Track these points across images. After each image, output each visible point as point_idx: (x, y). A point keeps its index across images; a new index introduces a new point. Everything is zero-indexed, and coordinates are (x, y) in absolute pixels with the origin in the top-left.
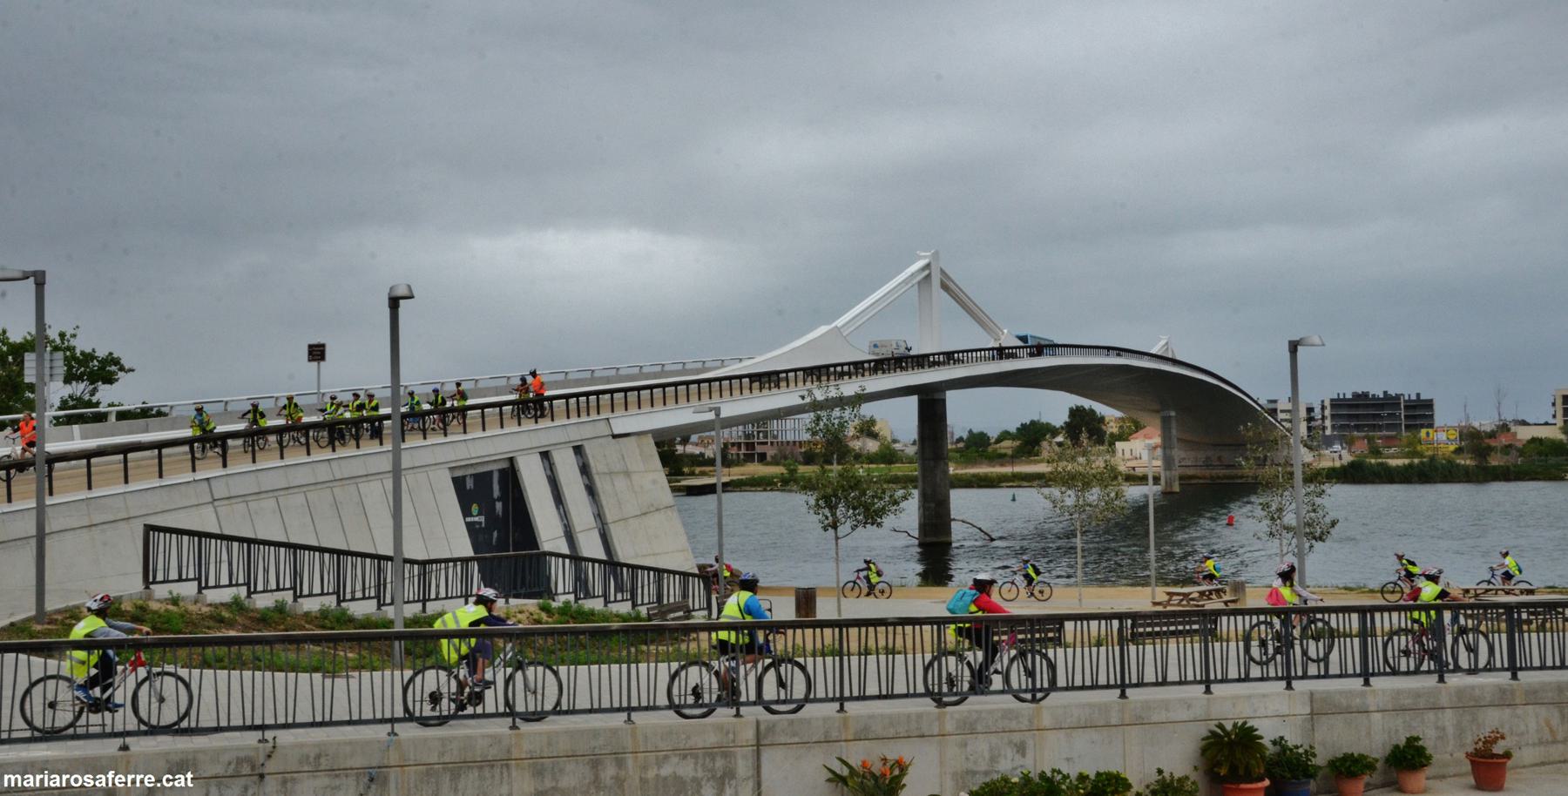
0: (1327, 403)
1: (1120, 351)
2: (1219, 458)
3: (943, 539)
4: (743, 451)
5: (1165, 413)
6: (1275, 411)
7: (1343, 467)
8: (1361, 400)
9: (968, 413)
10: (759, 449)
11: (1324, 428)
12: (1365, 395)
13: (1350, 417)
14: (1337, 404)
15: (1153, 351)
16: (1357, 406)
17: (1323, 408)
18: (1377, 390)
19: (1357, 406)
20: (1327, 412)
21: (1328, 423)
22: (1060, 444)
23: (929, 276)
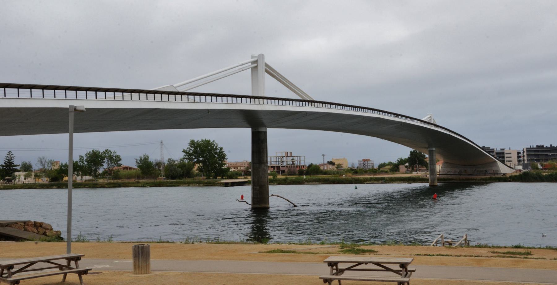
0: (525, 150)
1: (397, 115)
2: (465, 171)
3: (263, 206)
4: (276, 170)
5: (430, 149)
6: (503, 153)
7: (520, 175)
8: (540, 148)
9: (282, 143)
10: (282, 169)
11: (524, 160)
12: (542, 146)
13: (535, 155)
14: (529, 150)
15: (423, 119)
16: (538, 151)
17: (524, 152)
18: (547, 144)
19: (538, 151)
20: (525, 154)
21: (526, 158)
22: (406, 167)
23: (256, 67)
